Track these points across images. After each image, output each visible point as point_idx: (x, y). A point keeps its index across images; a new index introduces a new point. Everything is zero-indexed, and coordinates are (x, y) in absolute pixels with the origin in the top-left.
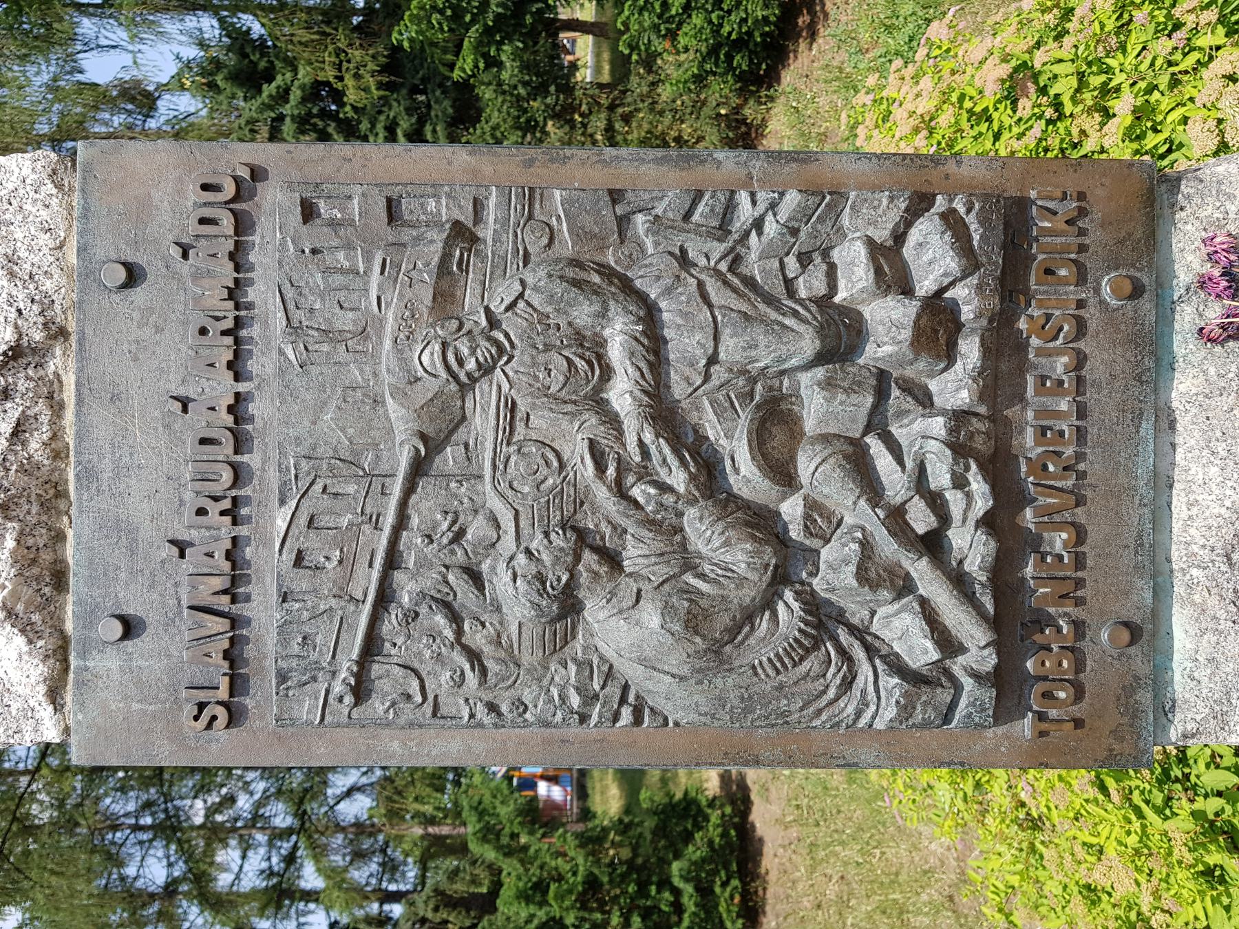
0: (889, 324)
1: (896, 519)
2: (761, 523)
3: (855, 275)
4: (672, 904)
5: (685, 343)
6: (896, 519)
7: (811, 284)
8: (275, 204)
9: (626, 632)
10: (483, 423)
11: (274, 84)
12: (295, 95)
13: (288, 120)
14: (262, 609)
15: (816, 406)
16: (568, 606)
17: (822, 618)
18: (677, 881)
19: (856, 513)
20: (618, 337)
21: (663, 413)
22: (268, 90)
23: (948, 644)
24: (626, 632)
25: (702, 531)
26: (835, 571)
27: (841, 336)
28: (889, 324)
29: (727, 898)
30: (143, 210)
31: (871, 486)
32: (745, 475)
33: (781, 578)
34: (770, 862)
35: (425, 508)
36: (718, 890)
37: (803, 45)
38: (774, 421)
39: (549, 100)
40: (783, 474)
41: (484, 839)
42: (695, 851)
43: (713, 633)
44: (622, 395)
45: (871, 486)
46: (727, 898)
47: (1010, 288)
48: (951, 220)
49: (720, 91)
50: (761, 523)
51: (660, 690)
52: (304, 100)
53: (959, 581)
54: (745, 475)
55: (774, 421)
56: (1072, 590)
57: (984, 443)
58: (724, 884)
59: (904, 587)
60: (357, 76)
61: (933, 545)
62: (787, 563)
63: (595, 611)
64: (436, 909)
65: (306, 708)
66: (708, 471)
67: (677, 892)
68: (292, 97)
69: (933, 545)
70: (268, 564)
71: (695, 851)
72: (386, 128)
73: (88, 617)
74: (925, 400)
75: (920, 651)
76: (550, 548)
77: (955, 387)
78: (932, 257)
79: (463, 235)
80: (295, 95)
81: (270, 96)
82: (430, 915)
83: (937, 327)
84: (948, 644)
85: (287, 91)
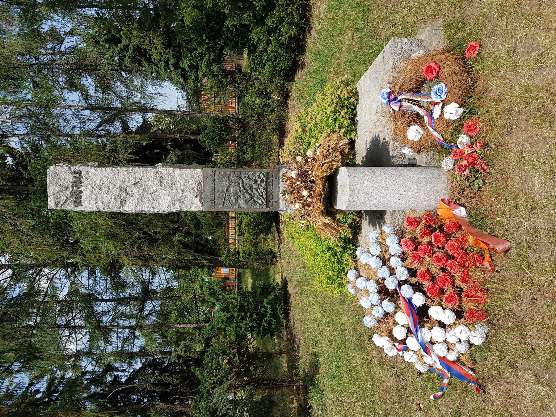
0: (259, 180)
1: (259, 194)
2: (250, 194)
3: (257, 178)
4: (264, 311)
5: (245, 182)
6: (259, 194)
7: (254, 178)
8: (217, 172)
9: (241, 202)
10: (231, 188)
11: (122, 44)
12: (131, 48)
13: (127, 57)
14: (216, 201)
15: (255, 187)
16: (237, 200)
17: (254, 201)
18: (266, 305)
19: (257, 194)
20: (240, 182)
21: (244, 187)
22: (120, 46)
23: (263, 203)
24: (241, 202)
25: (246, 195)
26: (255, 198)
27: (256, 181)
28: (259, 180)
29: (280, 307)
30: (208, 173)
31: (258, 192)
32: (249, 191)
33: (252, 198)
34: (292, 300)
35: (227, 193)
36: (277, 307)
37: (300, 70)
38: (251, 187)
39: (228, 80)
40: (252, 191)
41: (211, 296)
42: (271, 297)
43: (247, 202)
44: (241, 186)
45: (258, 192)
46: (280, 307)
47: (267, 178)
48: (263, 174)
49: (278, 81)
50: (250, 194)
51: (244, 206)
52: (134, 51)
53: (264, 198)
54: (249, 191)
55: (251, 187)
56: (272, 199)
57: (265, 189)
58: (279, 306)
59: (260, 199)
60: (156, 48)
61: (262, 196)
62: (252, 197)
63: (239, 200)
64: (185, 352)
65: (219, 207)
66: (247, 191)
67: (266, 308)
68: (129, 50)
69: (262, 196)
70: (217, 197)
71: (271, 297)
72: (165, 62)
73: (204, 201)
74: (262, 186)
75: (261, 203)
76: (236, 196)
77: (263, 185)
78: (262, 176)
79: (230, 175)
80: (131, 48)
81: (121, 49)
82: (183, 354)
83: (262, 181)
84: (263, 203)
85: (127, 47)
